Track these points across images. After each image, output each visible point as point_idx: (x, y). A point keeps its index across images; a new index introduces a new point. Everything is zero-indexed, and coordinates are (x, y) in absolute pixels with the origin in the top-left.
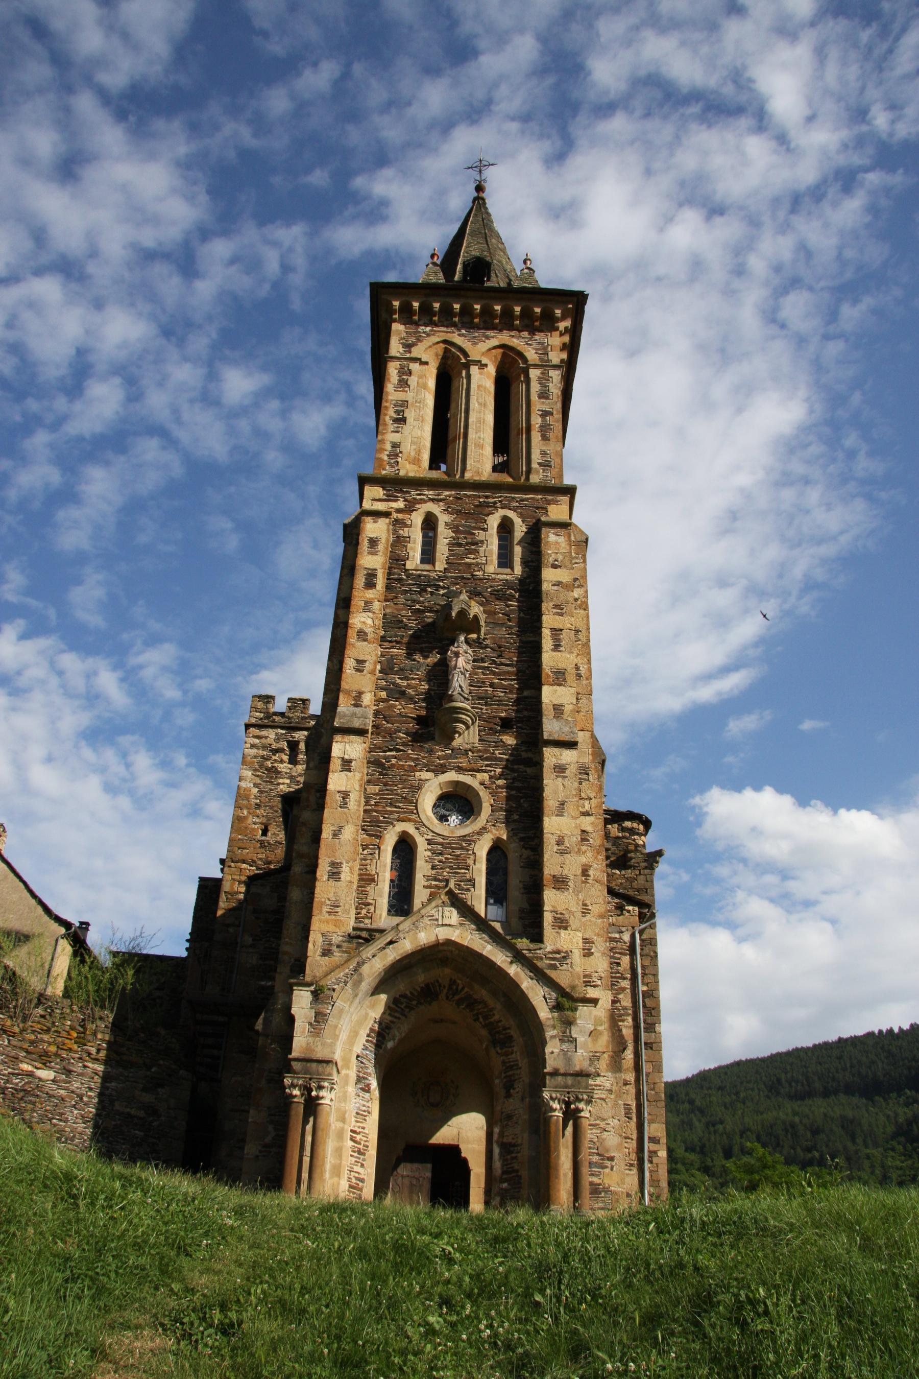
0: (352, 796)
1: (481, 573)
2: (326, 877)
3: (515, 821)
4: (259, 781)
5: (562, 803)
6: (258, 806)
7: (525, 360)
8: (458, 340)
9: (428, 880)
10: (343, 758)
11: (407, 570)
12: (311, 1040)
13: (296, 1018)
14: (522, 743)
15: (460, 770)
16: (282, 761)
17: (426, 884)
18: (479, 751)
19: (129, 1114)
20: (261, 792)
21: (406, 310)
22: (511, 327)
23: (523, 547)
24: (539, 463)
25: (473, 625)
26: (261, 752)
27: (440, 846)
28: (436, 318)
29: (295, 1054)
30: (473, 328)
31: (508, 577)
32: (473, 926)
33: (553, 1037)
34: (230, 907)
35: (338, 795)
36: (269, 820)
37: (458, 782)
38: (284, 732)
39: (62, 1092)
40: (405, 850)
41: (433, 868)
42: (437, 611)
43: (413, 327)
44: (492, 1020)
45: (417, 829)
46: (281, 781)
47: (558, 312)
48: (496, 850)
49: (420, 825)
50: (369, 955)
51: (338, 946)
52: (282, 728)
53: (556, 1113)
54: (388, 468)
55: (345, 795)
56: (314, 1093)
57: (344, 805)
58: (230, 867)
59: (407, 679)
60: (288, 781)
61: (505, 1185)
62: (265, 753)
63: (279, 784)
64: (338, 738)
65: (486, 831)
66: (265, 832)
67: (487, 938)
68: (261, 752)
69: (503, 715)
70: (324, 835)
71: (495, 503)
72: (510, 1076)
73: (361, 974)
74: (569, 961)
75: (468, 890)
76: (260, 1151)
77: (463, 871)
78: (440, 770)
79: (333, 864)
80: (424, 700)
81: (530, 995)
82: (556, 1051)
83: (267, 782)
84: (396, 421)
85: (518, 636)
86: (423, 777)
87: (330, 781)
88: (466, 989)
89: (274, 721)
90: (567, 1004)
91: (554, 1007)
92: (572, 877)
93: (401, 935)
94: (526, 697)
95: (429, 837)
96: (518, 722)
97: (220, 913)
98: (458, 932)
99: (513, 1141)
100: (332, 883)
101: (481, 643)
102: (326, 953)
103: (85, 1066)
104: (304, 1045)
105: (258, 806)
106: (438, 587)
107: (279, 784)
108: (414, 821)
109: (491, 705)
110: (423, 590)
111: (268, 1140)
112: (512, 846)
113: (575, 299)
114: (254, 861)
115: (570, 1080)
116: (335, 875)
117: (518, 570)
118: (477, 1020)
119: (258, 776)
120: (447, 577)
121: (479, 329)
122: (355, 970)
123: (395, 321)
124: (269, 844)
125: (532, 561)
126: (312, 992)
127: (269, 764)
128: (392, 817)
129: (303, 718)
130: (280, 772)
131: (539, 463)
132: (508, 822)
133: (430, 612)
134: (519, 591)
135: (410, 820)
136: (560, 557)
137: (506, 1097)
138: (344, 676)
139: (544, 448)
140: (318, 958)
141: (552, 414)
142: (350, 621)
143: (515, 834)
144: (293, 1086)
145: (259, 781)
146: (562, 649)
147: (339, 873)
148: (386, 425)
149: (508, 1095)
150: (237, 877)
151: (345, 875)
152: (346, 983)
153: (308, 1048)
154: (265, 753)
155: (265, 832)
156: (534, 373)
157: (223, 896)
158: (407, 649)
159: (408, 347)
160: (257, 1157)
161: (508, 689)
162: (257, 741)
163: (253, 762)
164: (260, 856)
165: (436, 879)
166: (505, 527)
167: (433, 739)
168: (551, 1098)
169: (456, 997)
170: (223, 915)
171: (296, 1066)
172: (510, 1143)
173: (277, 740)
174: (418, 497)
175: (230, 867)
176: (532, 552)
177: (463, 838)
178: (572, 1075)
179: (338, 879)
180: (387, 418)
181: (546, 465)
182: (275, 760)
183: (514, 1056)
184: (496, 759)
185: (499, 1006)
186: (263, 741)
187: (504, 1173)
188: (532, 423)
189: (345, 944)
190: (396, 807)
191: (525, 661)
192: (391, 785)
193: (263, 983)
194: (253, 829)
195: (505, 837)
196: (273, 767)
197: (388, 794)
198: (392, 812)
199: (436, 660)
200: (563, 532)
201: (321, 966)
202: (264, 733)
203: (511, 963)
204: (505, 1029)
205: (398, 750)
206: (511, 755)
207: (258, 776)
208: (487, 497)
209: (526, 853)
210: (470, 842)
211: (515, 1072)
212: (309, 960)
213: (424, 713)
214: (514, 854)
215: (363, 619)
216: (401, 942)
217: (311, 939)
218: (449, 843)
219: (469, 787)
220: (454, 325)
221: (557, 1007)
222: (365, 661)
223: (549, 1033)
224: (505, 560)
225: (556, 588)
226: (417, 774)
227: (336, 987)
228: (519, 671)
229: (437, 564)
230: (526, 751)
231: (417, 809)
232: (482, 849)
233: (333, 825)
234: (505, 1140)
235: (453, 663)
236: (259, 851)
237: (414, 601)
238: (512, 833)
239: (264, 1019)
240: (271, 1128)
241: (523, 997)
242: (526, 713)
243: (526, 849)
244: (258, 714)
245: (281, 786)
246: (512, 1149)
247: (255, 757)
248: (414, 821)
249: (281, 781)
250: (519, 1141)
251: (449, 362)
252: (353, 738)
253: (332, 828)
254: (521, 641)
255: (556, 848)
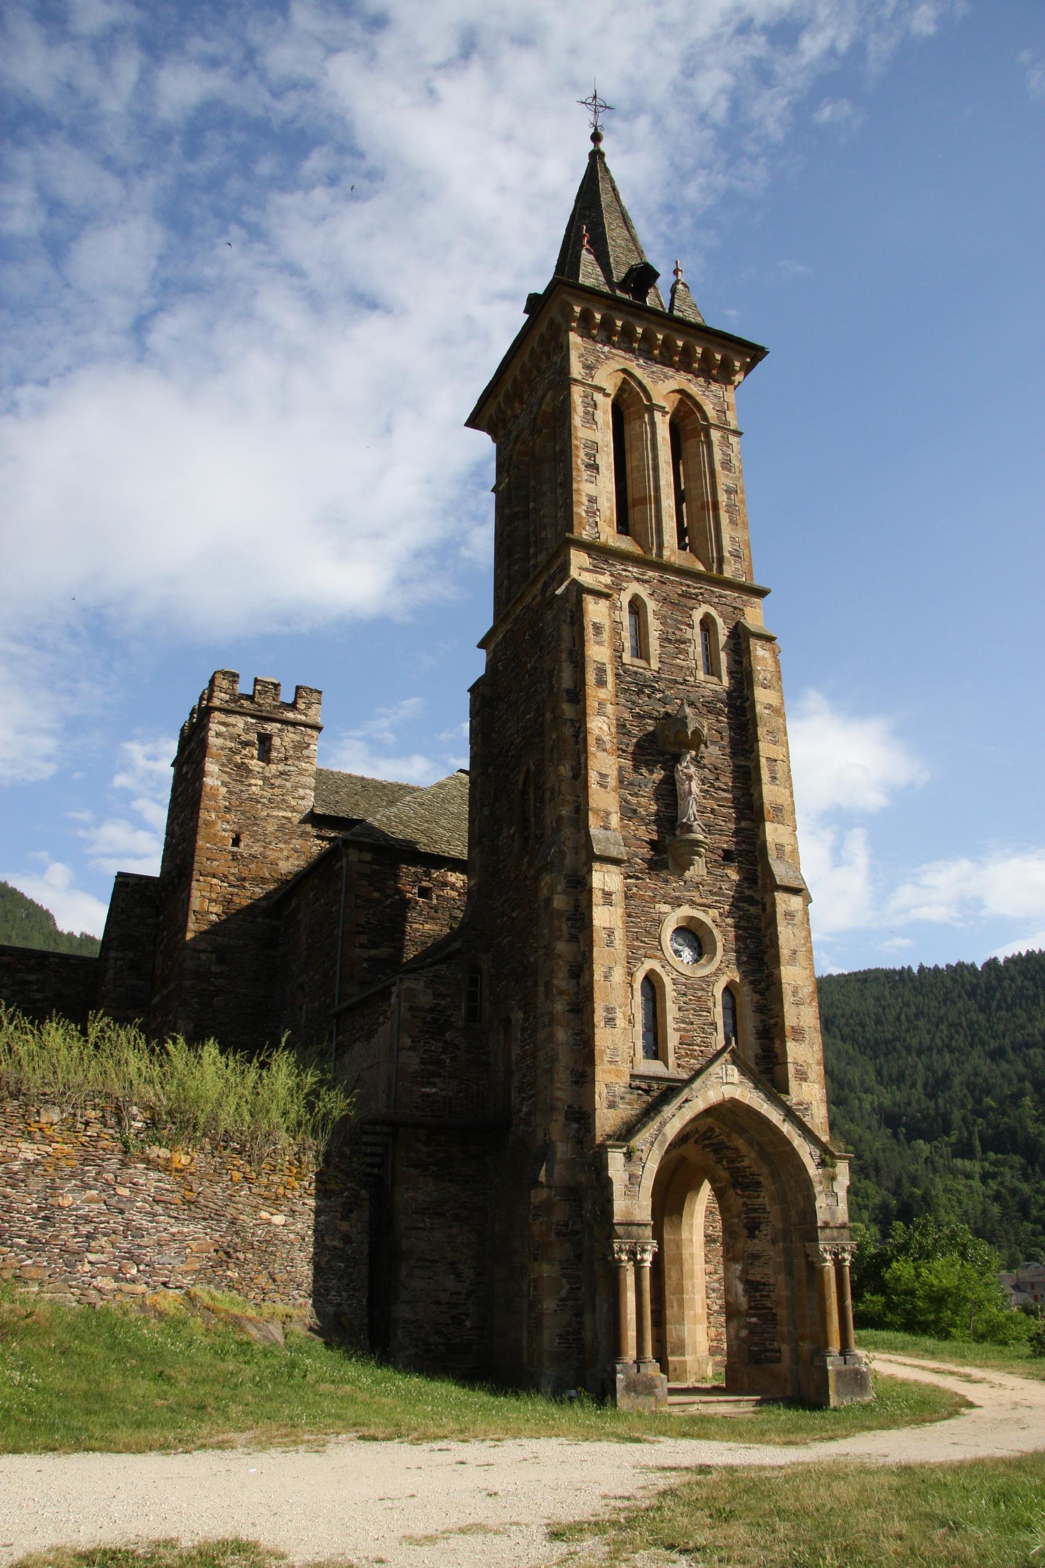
0: (616, 934)
1: (692, 679)
2: (602, 1024)
3: (744, 963)
4: (227, 780)
5: (794, 952)
6: (228, 809)
7: (705, 417)
8: (638, 373)
9: (677, 1022)
10: (603, 890)
11: (624, 664)
12: (628, 1202)
13: (614, 1180)
14: (745, 879)
15: (692, 903)
16: (252, 757)
17: (676, 1026)
18: (708, 885)
19: (334, 1247)
20: (230, 792)
21: (586, 318)
22: (688, 369)
23: (727, 654)
24: (730, 552)
25: (697, 740)
26: (229, 744)
27: (689, 988)
28: (615, 339)
29: (617, 1218)
30: (651, 360)
31: (718, 688)
32: (751, 1085)
33: (820, 1192)
34: (202, 929)
35: (604, 932)
36: (240, 827)
37: (693, 917)
38: (254, 721)
39: (292, 1236)
40: (652, 986)
41: (680, 1009)
42: (656, 719)
43: (590, 342)
44: (739, 1165)
45: (663, 967)
46: (253, 781)
47: (737, 364)
48: (729, 990)
49: (665, 962)
50: (670, 1115)
51: (622, 1098)
52: (253, 716)
53: (828, 1264)
54: (587, 528)
55: (610, 932)
56: (639, 1257)
57: (610, 944)
58: (198, 880)
59: (636, 795)
60: (261, 783)
61: (754, 1320)
62: (233, 745)
63: (250, 785)
64: (596, 866)
65: (722, 970)
66: (236, 842)
67: (763, 1096)
68: (229, 744)
69: (725, 846)
70: (596, 977)
71: (697, 595)
72: (753, 1218)
73: (664, 1134)
74: (809, 1113)
75: (711, 1034)
76: (558, 1306)
77: (705, 1013)
78: (677, 903)
79: (609, 1010)
80: (655, 822)
81: (801, 1152)
82: (824, 1205)
83: (237, 781)
84: (588, 466)
85: (731, 758)
86: (662, 910)
87: (595, 915)
88: (722, 1137)
89: (242, 706)
90: (828, 1159)
91: (819, 1164)
92: (807, 1029)
93: (694, 1094)
94: (743, 829)
95: (674, 977)
96: (740, 855)
97: (189, 936)
98: (739, 1090)
99: (762, 1280)
100: (608, 1030)
101: (699, 762)
102: (612, 1105)
103: (304, 1204)
104: (624, 1209)
105: (228, 809)
106: (654, 690)
107: (250, 785)
108: (661, 959)
109: (714, 834)
110: (640, 692)
111: (563, 1293)
112: (745, 988)
113: (753, 353)
114: (226, 876)
115: (835, 1232)
116: (610, 1021)
117: (726, 680)
118: (719, 1161)
119: (226, 773)
120: (661, 679)
121: (657, 362)
122: (660, 1130)
123: (573, 329)
124: (242, 856)
125: (736, 672)
126: (624, 1154)
127: (238, 759)
128: (639, 952)
129: (275, 707)
130: (251, 771)
131: (730, 552)
132: (739, 963)
133: (651, 718)
134: (727, 705)
135: (656, 957)
136: (769, 676)
137: (748, 1237)
138: (590, 791)
139: (733, 535)
140: (605, 1110)
141: (736, 492)
142: (588, 725)
143: (745, 977)
144: (621, 1250)
145: (227, 780)
146: (778, 782)
147: (613, 1019)
148: (579, 470)
149: (751, 1235)
150: (207, 894)
151: (621, 1022)
152: (652, 1144)
153: (628, 1212)
154: (233, 745)
155: (236, 842)
156: (715, 435)
157: (192, 918)
158: (634, 760)
159: (589, 368)
160: (555, 1311)
161: (726, 818)
162: (223, 729)
163: (219, 755)
164: (232, 871)
165: (683, 1022)
166: (707, 624)
167: (667, 868)
168: (825, 1250)
169: (706, 1142)
170: (193, 939)
171: (620, 1230)
172: (758, 1283)
173: (247, 731)
174: (624, 573)
175: (198, 880)
176: (735, 661)
177: (702, 978)
178: (837, 1228)
179: (614, 1026)
180: (579, 461)
181: (736, 556)
182: (245, 755)
183: (760, 1200)
184: (723, 895)
185: (753, 1155)
186: (231, 729)
187: (750, 1308)
188: (720, 499)
189: (628, 1096)
190: (642, 941)
191: (739, 788)
192: (635, 917)
193: (434, 1090)
194: (224, 837)
195: (738, 980)
196: (243, 763)
197: (633, 927)
198: (639, 948)
199: (661, 777)
200: (768, 645)
201: (607, 1119)
202: (231, 719)
203: (784, 1121)
204: (752, 1174)
205: (638, 878)
206: (736, 891)
207: (226, 773)
208: (688, 586)
209: (757, 997)
210: (708, 984)
211: (762, 1215)
212: (597, 1113)
213: (655, 838)
214: (746, 999)
215: (599, 725)
216: (695, 1100)
217: (597, 1090)
218: (692, 984)
219: (702, 924)
220: (631, 351)
221: (822, 1164)
222: (607, 776)
223: (818, 1188)
224: (712, 669)
225: (767, 711)
226: (657, 906)
227: (643, 1147)
228: (735, 798)
229: (652, 661)
230: (748, 888)
231: (660, 945)
232: (718, 990)
233: (603, 965)
234: (750, 1277)
235: (686, 786)
236: (231, 864)
237: (633, 703)
238: (744, 975)
239: (547, 1170)
240: (564, 1281)
241: (794, 1154)
242: (744, 846)
243: (756, 992)
244: (223, 695)
245: (254, 788)
246: (761, 1287)
247: (222, 749)
248: (661, 959)
249: (253, 781)
250: (772, 1281)
251: (625, 396)
252: (610, 867)
253: (603, 969)
254: (735, 765)
255: (792, 999)
